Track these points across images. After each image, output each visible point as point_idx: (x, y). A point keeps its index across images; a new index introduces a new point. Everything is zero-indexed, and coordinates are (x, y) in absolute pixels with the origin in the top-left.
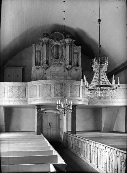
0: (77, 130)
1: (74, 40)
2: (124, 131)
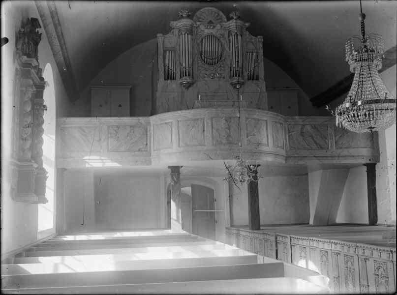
0: (261, 224)
1: (247, 24)
2: (367, 222)
